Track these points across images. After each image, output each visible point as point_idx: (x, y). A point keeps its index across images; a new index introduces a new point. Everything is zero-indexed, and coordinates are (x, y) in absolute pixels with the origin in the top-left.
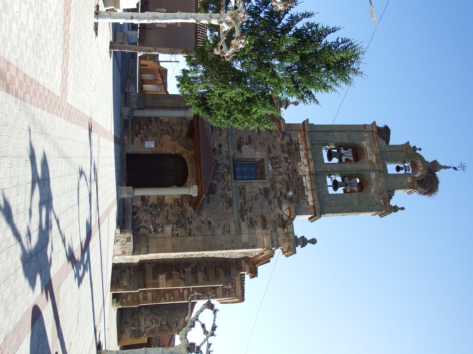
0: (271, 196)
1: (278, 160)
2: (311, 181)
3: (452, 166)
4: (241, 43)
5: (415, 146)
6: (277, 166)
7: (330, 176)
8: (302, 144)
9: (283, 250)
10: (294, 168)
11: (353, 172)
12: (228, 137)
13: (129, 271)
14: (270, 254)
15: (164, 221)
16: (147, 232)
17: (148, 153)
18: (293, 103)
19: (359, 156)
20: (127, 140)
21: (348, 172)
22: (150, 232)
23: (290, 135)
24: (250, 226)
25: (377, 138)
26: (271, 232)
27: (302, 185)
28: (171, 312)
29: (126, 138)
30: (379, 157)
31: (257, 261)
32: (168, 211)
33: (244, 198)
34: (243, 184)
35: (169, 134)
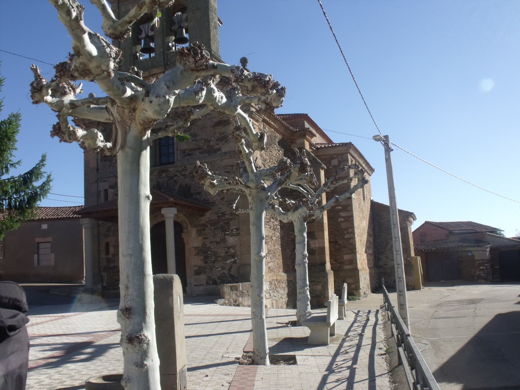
16: (235, 266)
22: (235, 262)
24: (226, 140)
28: (383, 230)
32: (211, 242)
33: (195, 150)
34: (179, 152)
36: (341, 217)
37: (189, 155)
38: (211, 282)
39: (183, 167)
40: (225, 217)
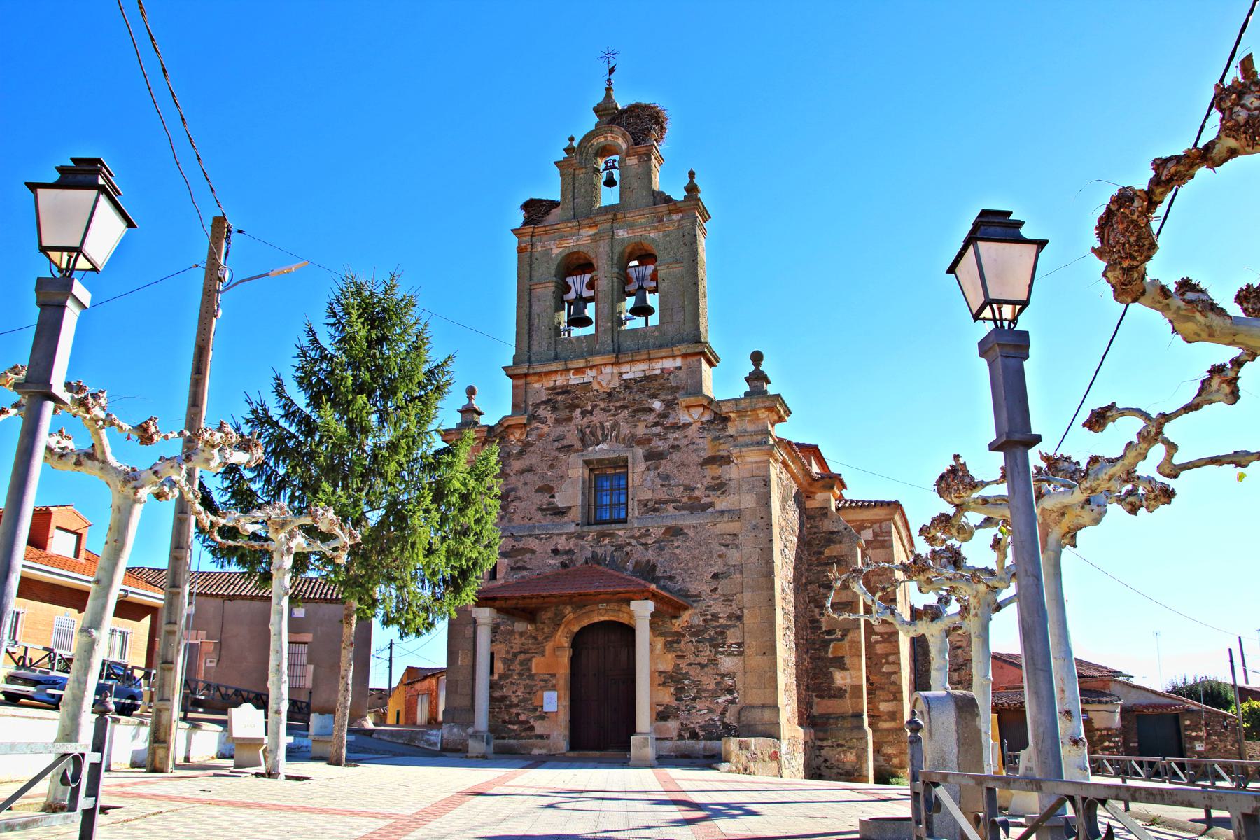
0: (662, 446)
1: (588, 431)
2: (632, 361)
3: (607, 77)
4: (323, 514)
5: (566, 150)
6: (599, 433)
7: (621, 323)
8: (555, 381)
9: (776, 422)
10: (605, 396)
11: (615, 275)
12: (537, 537)
13: (826, 749)
14: (786, 448)
15: (711, 671)
16: (733, 709)
17: (568, 703)
18: (470, 398)
19: (582, 261)
20: (540, 748)
21: (616, 284)
22: (733, 702)
23: (537, 406)
25: (545, 227)
26: (736, 446)
27: (639, 381)
29: (536, 752)
30: (585, 222)
31: (804, 476)
32: (690, 665)
33: (666, 502)
35: (530, 660)
36: (877, 634)
37: (655, 510)
38: (688, 735)
39: (643, 531)
40: (718, 622)
